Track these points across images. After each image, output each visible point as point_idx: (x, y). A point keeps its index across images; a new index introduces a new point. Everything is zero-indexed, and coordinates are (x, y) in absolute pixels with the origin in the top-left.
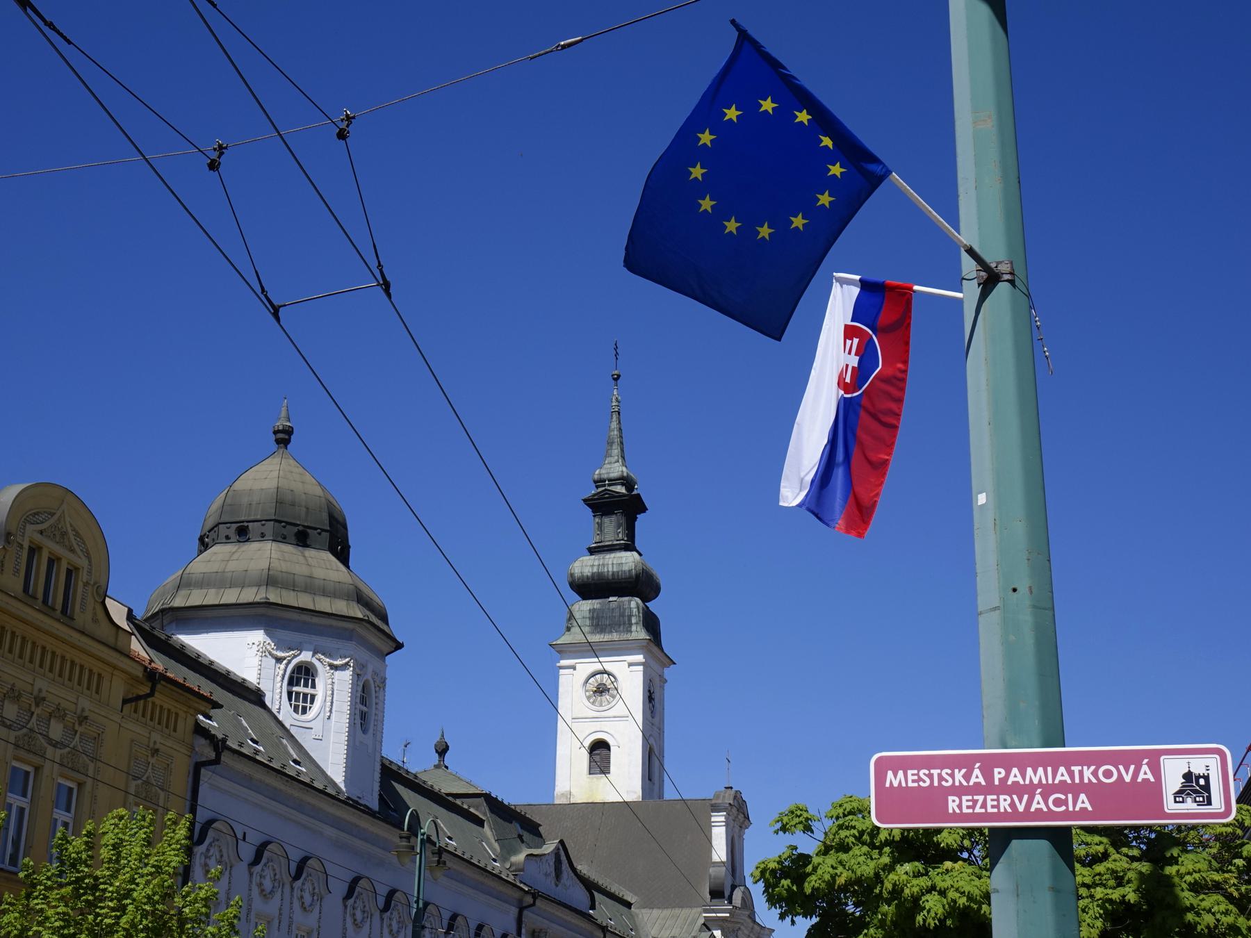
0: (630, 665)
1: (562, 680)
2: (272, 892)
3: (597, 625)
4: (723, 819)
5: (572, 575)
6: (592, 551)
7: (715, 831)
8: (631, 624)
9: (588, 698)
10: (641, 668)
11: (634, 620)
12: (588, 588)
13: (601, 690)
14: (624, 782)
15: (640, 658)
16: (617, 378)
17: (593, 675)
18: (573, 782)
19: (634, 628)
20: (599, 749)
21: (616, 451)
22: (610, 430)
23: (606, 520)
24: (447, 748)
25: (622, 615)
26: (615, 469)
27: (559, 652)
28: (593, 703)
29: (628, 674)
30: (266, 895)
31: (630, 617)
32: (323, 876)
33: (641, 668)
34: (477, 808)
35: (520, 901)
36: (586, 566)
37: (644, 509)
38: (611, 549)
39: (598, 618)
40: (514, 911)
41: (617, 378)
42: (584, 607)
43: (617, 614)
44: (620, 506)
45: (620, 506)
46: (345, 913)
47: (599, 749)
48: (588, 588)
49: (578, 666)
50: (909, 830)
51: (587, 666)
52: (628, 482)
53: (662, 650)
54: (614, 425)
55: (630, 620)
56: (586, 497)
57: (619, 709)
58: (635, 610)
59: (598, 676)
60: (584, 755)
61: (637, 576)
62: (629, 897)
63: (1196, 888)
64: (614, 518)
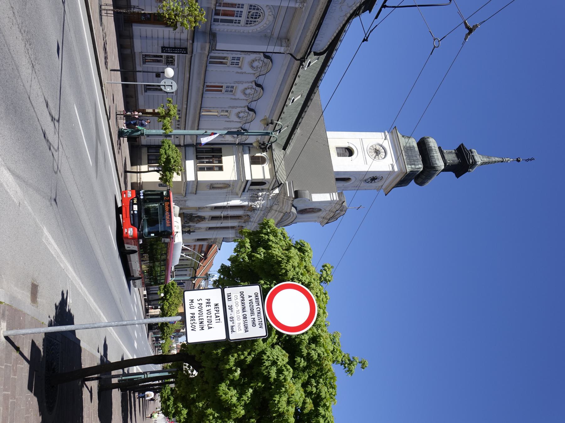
2: (239, 117)
3: (408, 150)
4: (335, 199)
5: (428, 138)
6: (439, 148)
7: (328, 195)
8: (411, 165)
9: (372, 146)
10: (391, 170)
11: (413, 166)
12: (423, 146)
13: (377, 152)
15: (396, 169)
16: (518, 161)
17: (384, 148)
18: (336, 139)
19: (410, 166)
20: (349, 152)
21: (486, 160)
22: (495, 156)
23: (454, 155)
25: (414, 161)
26: (479, 159)
28: (370, 148)
29: (386, 164)
30: (238, 115)
31: (414, 164)
32: (257, 98)
36: (433, 143)
37: (458, 176)
38: (443, 157)
39: (411, 150)
41: (518, 161)
42: (413, 143)
43: (415, 158)
44: (462, 164)
45: (462, 164)
46: (248, 82)
47: (349, 152)
48: (423, 146)
49: (386, 141)
51: (387, 144)
52: (475, 163)
53: (393, 188)
54: (497, 159)
55: (413, 164)
56: (464, 145)
57: (369, 160)
58: (418, 167)
60: (346, 145)
61: (434, 167)
62: (289, 150)
64: (456, 159)
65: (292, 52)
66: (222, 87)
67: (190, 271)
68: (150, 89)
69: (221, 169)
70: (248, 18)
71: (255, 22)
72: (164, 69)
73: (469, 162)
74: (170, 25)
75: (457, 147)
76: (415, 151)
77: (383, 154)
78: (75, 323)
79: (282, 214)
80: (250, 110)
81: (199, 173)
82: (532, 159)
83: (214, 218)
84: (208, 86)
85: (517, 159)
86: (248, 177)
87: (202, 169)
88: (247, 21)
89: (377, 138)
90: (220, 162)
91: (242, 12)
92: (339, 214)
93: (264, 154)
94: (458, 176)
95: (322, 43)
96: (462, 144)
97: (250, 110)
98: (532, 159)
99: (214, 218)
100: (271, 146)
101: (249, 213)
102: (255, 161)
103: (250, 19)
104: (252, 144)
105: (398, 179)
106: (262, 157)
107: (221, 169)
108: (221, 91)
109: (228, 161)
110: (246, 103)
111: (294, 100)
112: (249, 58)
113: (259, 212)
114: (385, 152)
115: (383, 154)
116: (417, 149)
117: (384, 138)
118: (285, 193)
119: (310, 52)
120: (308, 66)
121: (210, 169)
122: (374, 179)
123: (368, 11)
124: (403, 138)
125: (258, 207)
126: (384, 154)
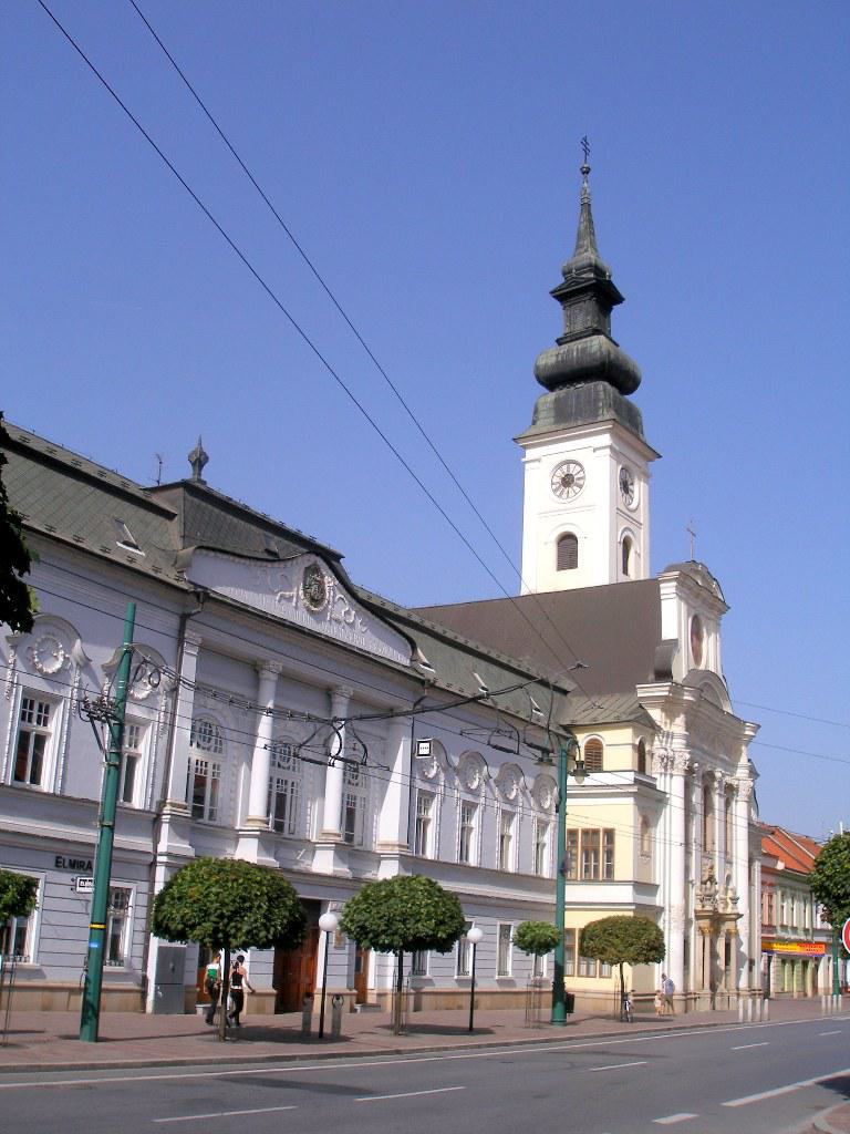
6: (560, 342)
8: (597, 409)
9: (555, 491)
13: (567, 481)
17: (560, 466)
18: (539, 575)
37: (618, 299)
41: (586, 172)
56: (552, 289)
59: (565, 467)
62: (567, 685)
69: (610, 834)
70: (209, 749)
73: (590, 279)
74: (430, 942)
75: (558, 303)
76: (566, 398)
77: (574, 469)
78: (623, 293)
81: (618, 876)
82: (585, 142)
85: (584, 173)
86: (631, 776)
87: (610, 870)
88: (215, 751)
93: (582, 739)
94: (618, 299)
96: (551, 293)
98: (585, 142)
102: (594, 761)
103: (213, 742)
105: (627, 435)
106: (587, 748)
111: (483, 688)
114: (568, 462)
120: (429, 666)
126: (572, 466)
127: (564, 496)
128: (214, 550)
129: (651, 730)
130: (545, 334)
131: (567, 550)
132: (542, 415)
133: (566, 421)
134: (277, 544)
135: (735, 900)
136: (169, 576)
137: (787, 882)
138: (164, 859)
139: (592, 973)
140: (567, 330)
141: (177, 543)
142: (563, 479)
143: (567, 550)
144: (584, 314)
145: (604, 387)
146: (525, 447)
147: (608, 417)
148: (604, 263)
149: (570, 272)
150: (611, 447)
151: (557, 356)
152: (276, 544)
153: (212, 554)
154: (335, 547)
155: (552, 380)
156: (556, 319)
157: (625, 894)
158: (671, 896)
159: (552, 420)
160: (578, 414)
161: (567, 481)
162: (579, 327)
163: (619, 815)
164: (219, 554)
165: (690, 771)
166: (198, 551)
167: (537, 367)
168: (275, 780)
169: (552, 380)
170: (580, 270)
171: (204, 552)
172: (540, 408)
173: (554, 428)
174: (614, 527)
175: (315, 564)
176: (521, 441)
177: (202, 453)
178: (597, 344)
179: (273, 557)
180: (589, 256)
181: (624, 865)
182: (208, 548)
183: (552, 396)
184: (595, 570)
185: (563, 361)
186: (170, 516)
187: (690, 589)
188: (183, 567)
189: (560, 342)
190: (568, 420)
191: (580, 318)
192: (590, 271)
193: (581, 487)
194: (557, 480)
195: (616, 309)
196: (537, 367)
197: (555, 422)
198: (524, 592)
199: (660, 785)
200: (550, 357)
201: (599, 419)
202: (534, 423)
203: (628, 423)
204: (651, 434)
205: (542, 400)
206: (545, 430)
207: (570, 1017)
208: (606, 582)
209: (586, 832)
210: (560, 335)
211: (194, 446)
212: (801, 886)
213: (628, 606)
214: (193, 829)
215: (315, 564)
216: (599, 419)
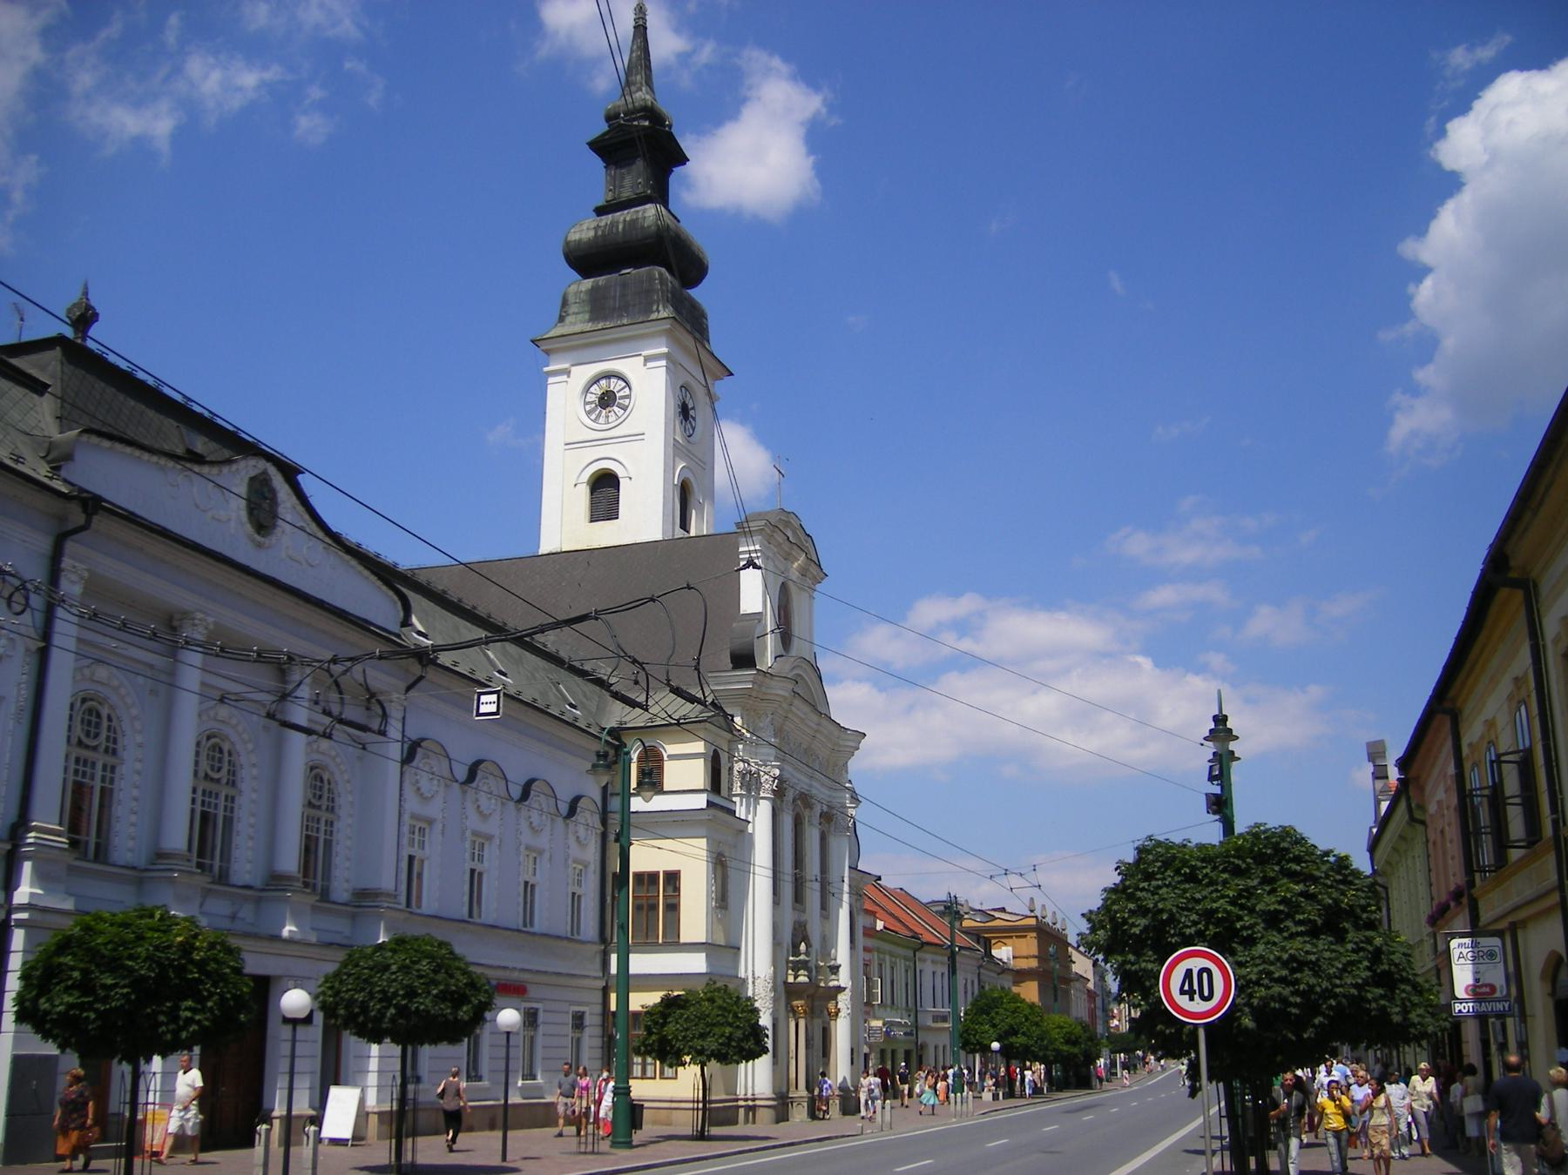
0: (647, 359)
1: (550, 389)
6: (600, 211)
9: (588, 413)
10: (664, 363)
13: (607, 400)
14: (643, 517)
17: (596, 380)
18: (564, 525)
24: (95, 317)
27: (547, 352)
29: (648, 378)
33: (664, 363)
34: (43, 369)
35: (62, 519)
40: (44, 544)
47: (605, 487)
50: (1209, 1068)
59: (603, 382)
60: (584, 492)
63: (1256, 924)
65: (403, 686)
66: (473, 871)
67: (924, 961)
68: (476, 1068)
69: (673, 878)
71: (110, 719)
72: (496, 1032)
77: (616, 385)
79: (797, 702)
80: (525, 795)
83: (798, 897)
84: (471, 915)
86: (700, 801)
89: (566, 395)
90: (653, 877)
91: (204, 792)
92: (794, 532)
95: (376, 604)
97: (525, 795)
99: (798, 897)
100: (612, 732)
101: (790, 795)
102: (652, 780)
104: (605, 789)
105: (689, 341)
107: (673, 878)
108: (480, 874)
109: (645, 857)
110: (560, 820)
111: (420, 633)
112: (412, 804)
113: (786, 767)
114: (608, 376)
115: (616, 385)
116: (602, 280)
117: (564, 378)
118: (745, 694)
119: (398, 636)
121: (673, 908)
122: (685, 412)
123: (300, 477)
124: (568, 319)
125: (777, 772)
127: (602, 420)
128: (110, 437)
129: (729, 736)
130: (580, 201)
131: (604, 490)
132: (573, 309)
133: (605, 319)
134: (208, 440)
135: (835, 969)
136: (41, 472)
137: (887, 946)
138: (24, 916)
139: (649, 1073)
140: (610, 196)
141: (52, 430)
142: (601, 398)
143: (604, 490)
144: (634, 179)
145: (661, 274)
146: (547, 352)
147: (664, 314)
148: (664, 107)
149: (617, 116)
150: (667, 356)
151: (596, 229)
152: (201, 444)
153: (106, 443)
154: (293, 453)
155: (586, 260)
156: (595, 179)
157: (696, 963)
158: (757, 967)
159: (587, 316)
160: (624, 309)
161: (607, 400)
162: (626, 194)
163: (688, 859)
164: (118, 446)
165: (779, 793)
166: (85, 438)
167: (567, 243)
168: (200, 792)
169: (586, 260)
170: (632, 113)
171: (95, 439)
172: (571, 299)
173: (589, 326)
174: (669, 468)
175: (265, 472)
176: (544, 346)
177: (89, 307)
178: (649, 213)
179: (195, 458)
180: (642, 96)
181: (694, 919)
182: (100, 434)
183: (588, 284)
184: (643, 517)
185: (603, 235)
186: (39, 387)
187: (779, 545)
188: (58, 459)
189: (600, 211)
190: (611, 316)
191: (628, 182)
192: (645, 118)
193: (625, 408)
194: (591, 398)
195: (678, 171)
196: (567, 243)
197: (591, 320)
198: (545, 548)
199: (741, 812)
200: (585, 230)
201: (654, 316)
202: (561, 319)
203: (693, 322)
204: (719, 341)
205: (573, 288)
206: (577, 328)
207: (637, 1137)
208: (659, 537)
209: (666, 873)
210: (601, 202)
211: (76, 297)
212: (900, 951)
213: (681, 575)
214: (71, 869)
215: (265, 472)
216: (654, 316)
